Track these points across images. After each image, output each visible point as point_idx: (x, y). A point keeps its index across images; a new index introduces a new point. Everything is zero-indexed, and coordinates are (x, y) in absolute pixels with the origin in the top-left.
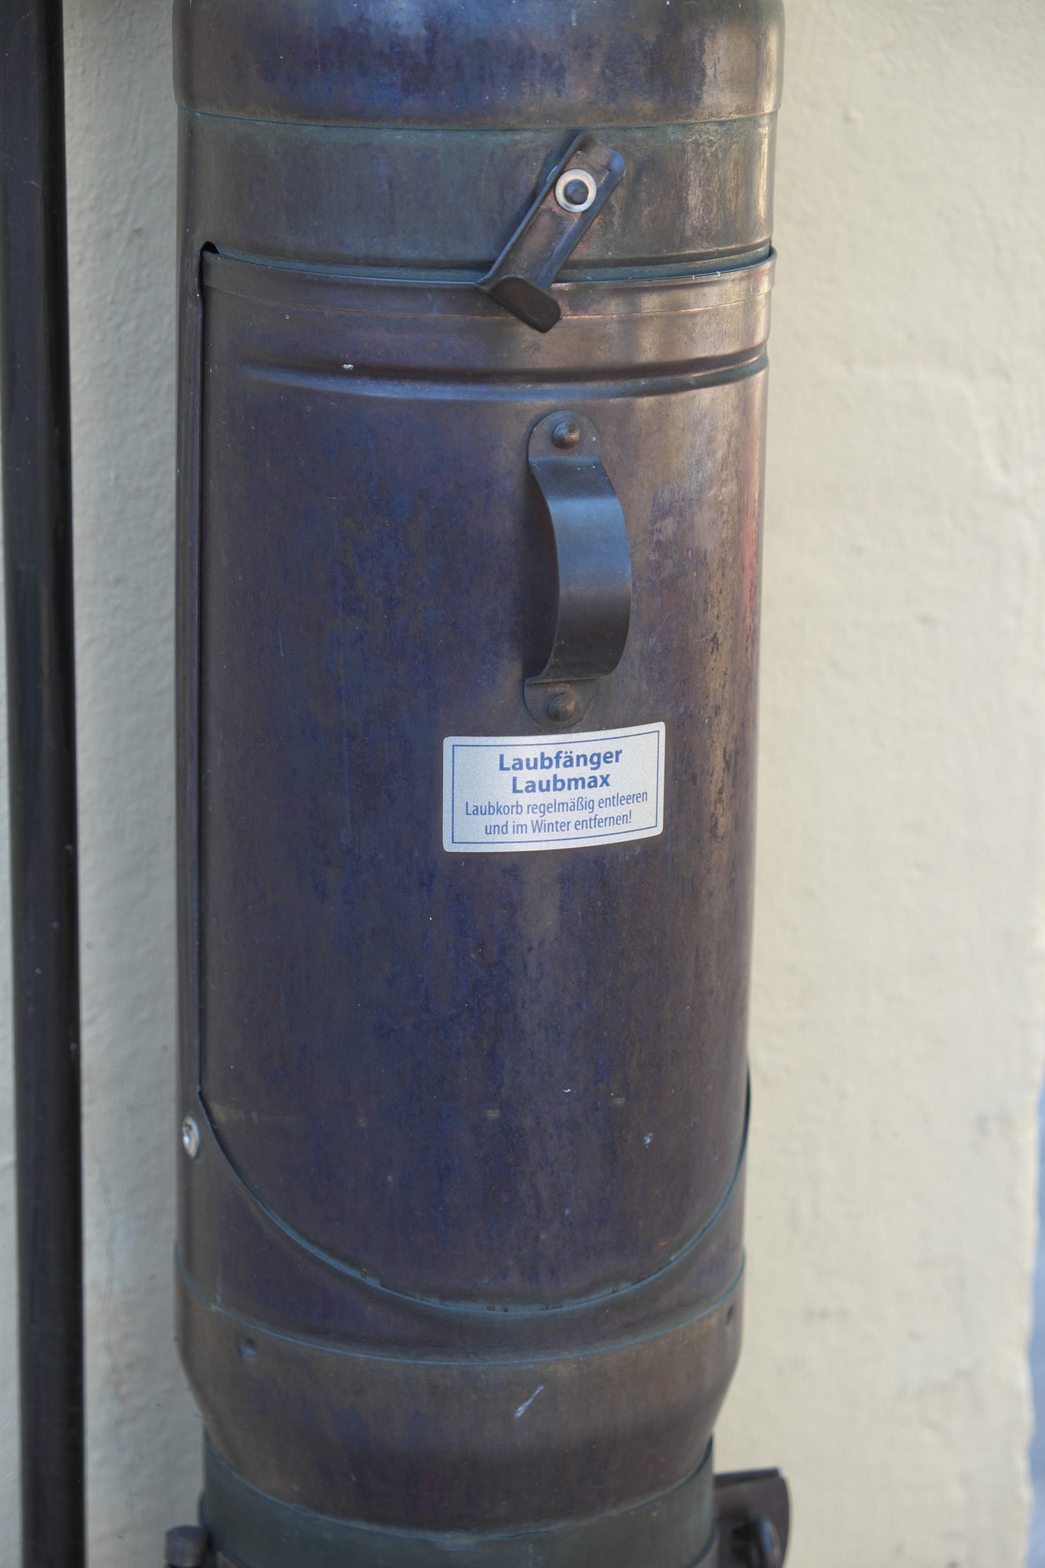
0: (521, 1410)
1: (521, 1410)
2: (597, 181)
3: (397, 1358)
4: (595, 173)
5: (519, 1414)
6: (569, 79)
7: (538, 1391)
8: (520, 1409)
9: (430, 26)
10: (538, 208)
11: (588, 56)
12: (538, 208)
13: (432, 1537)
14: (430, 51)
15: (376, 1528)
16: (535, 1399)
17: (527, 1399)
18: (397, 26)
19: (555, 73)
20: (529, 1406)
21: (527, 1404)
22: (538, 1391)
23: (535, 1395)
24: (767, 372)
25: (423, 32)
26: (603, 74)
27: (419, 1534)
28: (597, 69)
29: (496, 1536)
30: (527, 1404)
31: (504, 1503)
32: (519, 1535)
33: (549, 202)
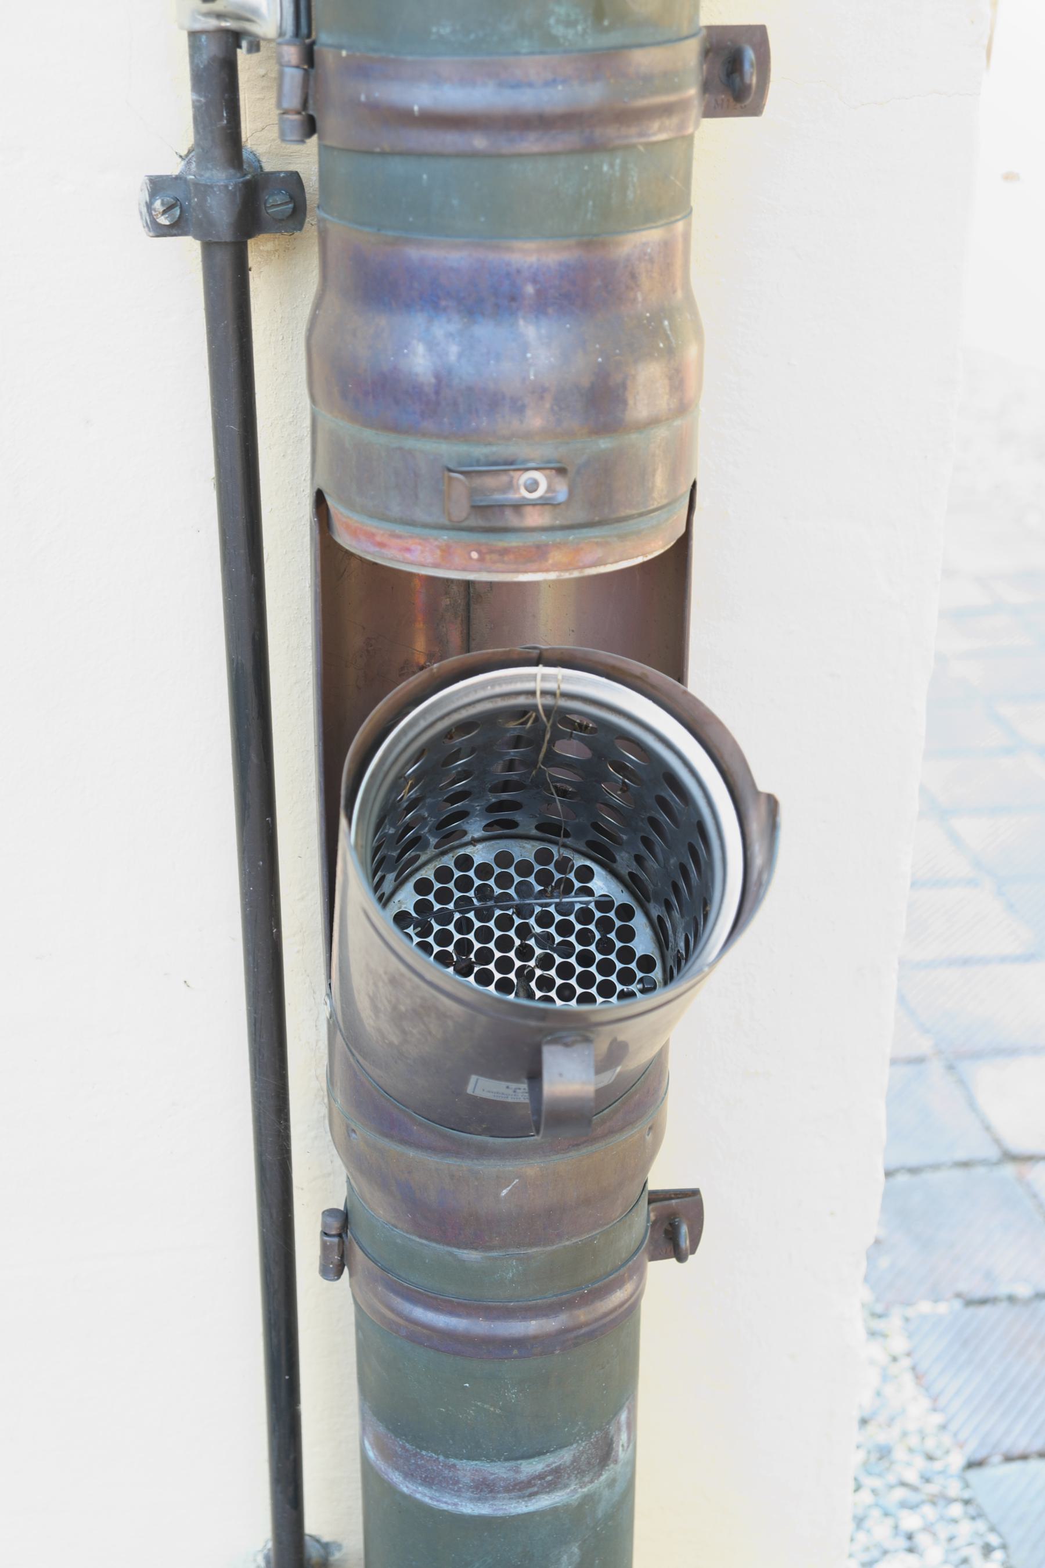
0: (504, 1192)
1: (504, 1192)
2: (547, 492)
3: (431, 1157)
4: (550, 489)
5: (503, 1194)
6: (529, 413)
7: (515, 1182)
8: (504, 1191)
9: (438, 377)
10: (509, 470)
11: (542, 398)
12: (509, 470)
13: (455, 1250)
14: (437, 393)
15: (424, 1241)
16: (513, 1186)
17: (509, 1186)
18: (417, 375)
19: (519, 408)
20: (510, 1190)
21: (509, 1188)
22: (515, 1182)
23: (513, 1184)
24: (689, 225)
25: (433, 380)
26: (552, 409)
27: (449, 1249)
28: (548, 406)
29: (494, 1254)
30: (509, 1188)
31: (497, 1239)
32: (508, 1255)
33: (516, 474)
